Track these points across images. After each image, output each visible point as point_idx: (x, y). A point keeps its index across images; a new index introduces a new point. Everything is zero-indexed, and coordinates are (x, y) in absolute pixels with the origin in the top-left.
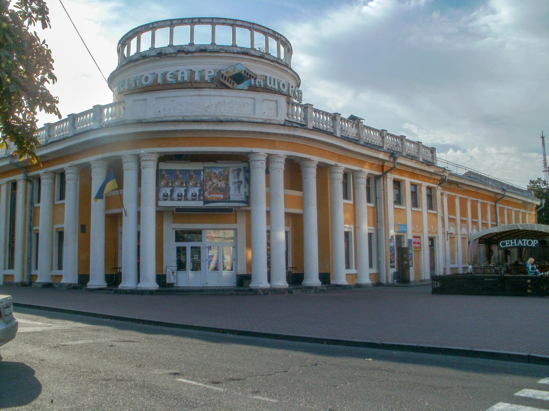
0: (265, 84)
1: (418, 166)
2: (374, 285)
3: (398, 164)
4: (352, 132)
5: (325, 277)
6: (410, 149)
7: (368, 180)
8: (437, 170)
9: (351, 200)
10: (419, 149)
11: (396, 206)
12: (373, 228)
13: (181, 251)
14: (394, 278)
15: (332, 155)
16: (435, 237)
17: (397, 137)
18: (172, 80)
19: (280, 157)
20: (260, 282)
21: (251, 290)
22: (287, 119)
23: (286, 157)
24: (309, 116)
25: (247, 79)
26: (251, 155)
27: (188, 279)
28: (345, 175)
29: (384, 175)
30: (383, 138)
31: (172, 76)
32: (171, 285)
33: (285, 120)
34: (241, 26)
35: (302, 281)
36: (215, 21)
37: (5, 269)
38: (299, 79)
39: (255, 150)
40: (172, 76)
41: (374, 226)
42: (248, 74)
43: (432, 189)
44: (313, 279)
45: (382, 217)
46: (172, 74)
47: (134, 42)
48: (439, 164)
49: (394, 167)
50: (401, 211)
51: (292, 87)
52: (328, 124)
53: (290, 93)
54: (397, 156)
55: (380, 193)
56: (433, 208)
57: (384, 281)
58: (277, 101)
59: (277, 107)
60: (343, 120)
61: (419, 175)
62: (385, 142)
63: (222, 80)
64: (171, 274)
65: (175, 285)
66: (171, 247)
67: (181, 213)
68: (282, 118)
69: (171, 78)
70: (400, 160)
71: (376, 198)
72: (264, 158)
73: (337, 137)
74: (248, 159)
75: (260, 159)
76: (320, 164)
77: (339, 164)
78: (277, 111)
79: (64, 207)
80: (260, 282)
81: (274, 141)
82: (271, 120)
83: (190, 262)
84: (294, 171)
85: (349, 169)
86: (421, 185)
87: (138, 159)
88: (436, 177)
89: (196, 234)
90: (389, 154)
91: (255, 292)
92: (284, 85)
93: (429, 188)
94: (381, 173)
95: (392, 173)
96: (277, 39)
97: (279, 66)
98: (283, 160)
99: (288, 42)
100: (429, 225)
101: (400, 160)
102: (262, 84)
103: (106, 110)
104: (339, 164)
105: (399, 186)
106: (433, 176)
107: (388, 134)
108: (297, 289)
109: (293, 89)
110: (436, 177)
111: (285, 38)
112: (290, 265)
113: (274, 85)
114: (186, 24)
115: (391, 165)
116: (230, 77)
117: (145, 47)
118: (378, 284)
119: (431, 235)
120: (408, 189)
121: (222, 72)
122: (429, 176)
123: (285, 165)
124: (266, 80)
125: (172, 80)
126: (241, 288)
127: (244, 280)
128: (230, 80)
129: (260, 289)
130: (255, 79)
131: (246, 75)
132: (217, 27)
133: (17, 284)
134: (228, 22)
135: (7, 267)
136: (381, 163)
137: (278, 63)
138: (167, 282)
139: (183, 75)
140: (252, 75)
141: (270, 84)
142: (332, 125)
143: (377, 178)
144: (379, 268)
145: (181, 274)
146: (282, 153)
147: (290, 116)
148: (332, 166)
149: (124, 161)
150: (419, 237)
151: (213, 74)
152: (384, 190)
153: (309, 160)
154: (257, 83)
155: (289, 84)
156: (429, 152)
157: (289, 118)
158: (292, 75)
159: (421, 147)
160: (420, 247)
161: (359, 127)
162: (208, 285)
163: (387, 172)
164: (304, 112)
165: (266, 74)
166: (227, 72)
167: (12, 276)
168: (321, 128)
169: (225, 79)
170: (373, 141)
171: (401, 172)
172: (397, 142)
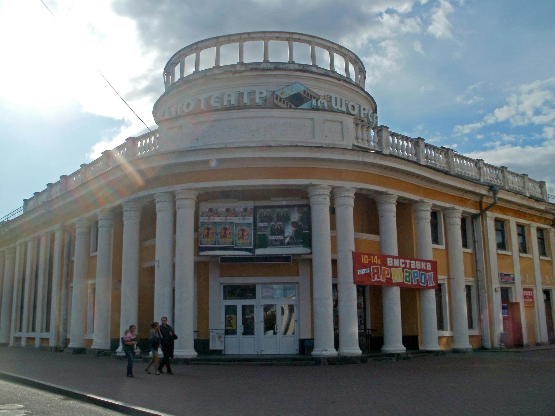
0: (330, 106)
1: (525, 202)
2: (475, 350)
3: (500, 199)
4: (440, 161)
5: (411, 341)
6: (514, 183)
7: (463, 220)
8: (549, 207)
9: (442, 245)
10: (524, 183)
11: (500, 252)
12: (471, 279)
13: (230, 310)
14: (502, 341)
15: (415, 189)
16: (551, 290)
17: (496, 168)
18: (217, 105)
19: (347, 190)
20: (325, 348)
21: (313, 359)
22: (356, 144)
23: (355, 191)
24: (384, 141)
25: (308, 100)
26: (311, 188)
27: (239, 345)
28: (434, 215)
29: (482, 214)
30: (479, 169)
31: (217, 100)
32: (219, 352)
33: (354, 145)
34: (299, 40)
35: (382, 346)
36: (267, 35)
37: (42, 332)
38: (375, 103)
39: (315, 182)
40: (217, 100)
41: (473, 277)
42: (308, 94)
43: (544, 232)
44: (395, 344)
45: (482, 264)
46: (216, 98)
47: (178, 68)
48: (550, 200)
49: (495, 203)
50: (506, 257)
51: (364, 109)
52: (410, 151)
53: (362, 116)
54: (498, 189)
55: (479, 236)
56: (547, 253)
57: (488, 345)
58: (341, 122)
59: (342, 128)
60: (428, 147)
61: (526, 213)
62: (482, 174)
63: (276, 102)
64: (217, 338)
65: (223, 353)
66: (218, 304)
67: (229, 264)
68: (349, 142)
69: (216, 102)
70: (500, 195)
71: (475, 242)
72: (328, 192)
73: (420, 165)
74: (307, 194)
75: (321, 193)
76: (401, 201)
77: (425, 200)
78: (343, 134)
79: (96, 260)
80: (325, 348)
81: (339, 171)
82: (335, 144)
83: (241, 324)
84: (368, 210)
85: (439, 207)
86: (529, 226)
87: (173, 197)
88: (548, 216)
89: (4, 261)
90: (488, 187)
91: (318, 361)
92: (353, 106)
93: (540, 230)
94: (479, 212)
95: (492, 211)
96: (344, 56)
97: (347, 85)
98: (352, 195)
99: (359, 59)
100: (543, 274)
101: (500, 195)
102: (326, 105)
103: (139, 143)
104: (425, 200)
105: (503, 226)
106: (544, 215)
107: (486, 165)
108: (373, 357)
109: (366, 112)
110: (548, 216)
111: (354, 54)
112: (369, 326)
113: (341, 106)
114: (233, 41)
115: (491, 201)
116: (286, 99)
117: (190, 70)
118: (483, 349)
119: (546, 287)
120: (514, 231)
121: (277, 93)
122: (540, 215)
123: (355, 201)
124: (331, 101)
125: (217, 105)
126: (303, 357)
127: (306, 346)
128: (286, 101)
129: (324, 358)
130: (317, 100)
131: (306, 96)
132: (271, 43)
133: (51, 349)
134: (283, 35)
135: (44, 331)
136: (478, 199)
137: (345, 81)
138: (210, 348)
139: (229, 99)
140: (313, 95)
141: (336, 105)
142: (414, 152)
143: (474, 217)
144: (481, 329)
145: (230, 338)
146: (350, 188)
147: (360, 140)
148: (416, 202)
149: (156, 201)
150: (531, 290)
151: (265, 95)
152: (483, 232)
153: (386, 194)
154: (319, 104)
155: (360, 106)
156: (537, 187)
157: (358, 142)
158: (365, 97)
159: (527, 180)
160: (533, 302)
161: (448, 156)
162: (263, 353)
163: (487, 209)
164: (378, 136)
165: (331, 94)
166: (282, 93)
167: (47, 339)
168: (401, 156)
169: (277, 99)
170: (467, 173)
171: (503, 210)
172: (496, 174)
